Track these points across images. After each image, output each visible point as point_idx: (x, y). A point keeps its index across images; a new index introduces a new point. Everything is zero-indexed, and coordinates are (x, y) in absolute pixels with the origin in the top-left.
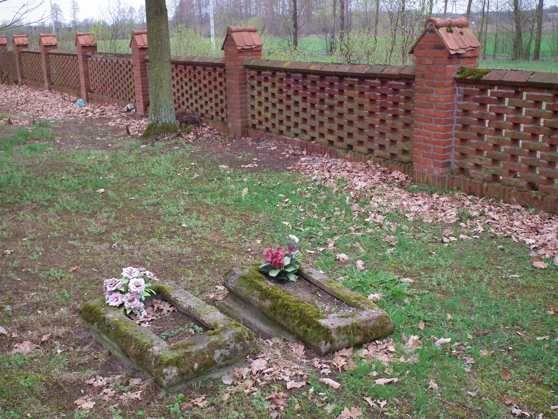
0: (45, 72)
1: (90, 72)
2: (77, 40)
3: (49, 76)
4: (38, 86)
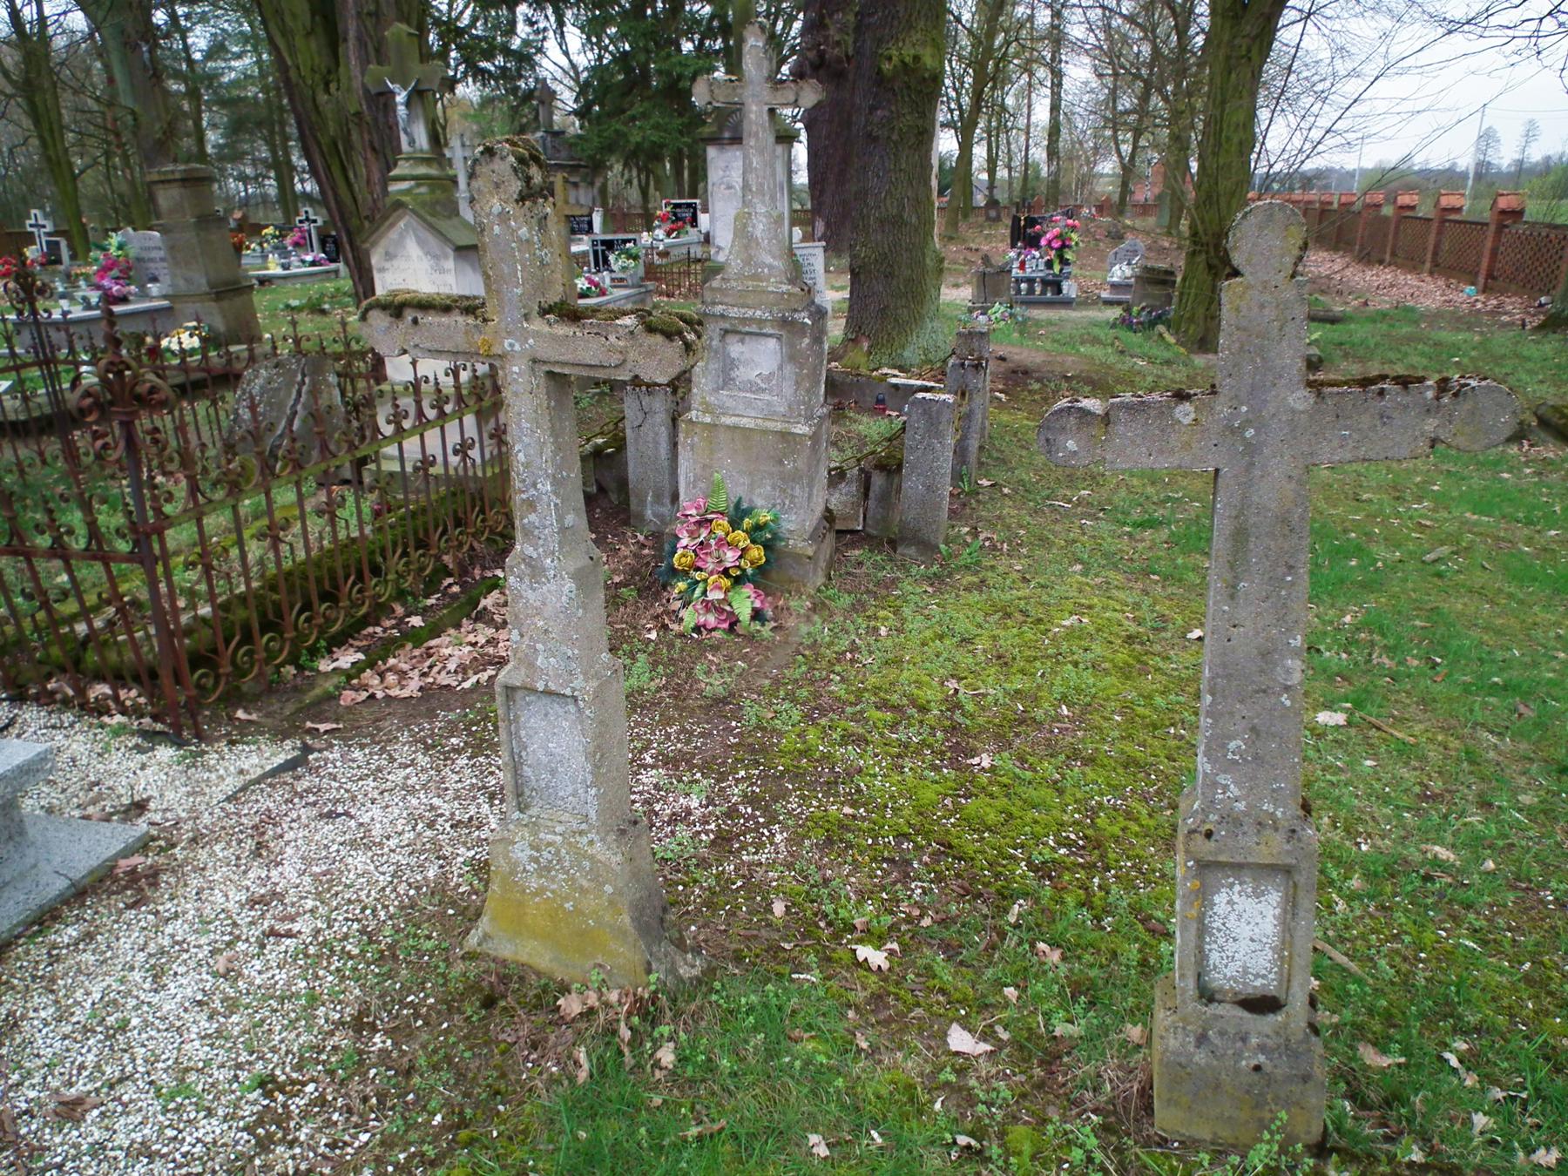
0: (1431, 248)
1: (1502, 249)
2: (1495, 202)
3: (1435, 254)
4: (1001, 894)
